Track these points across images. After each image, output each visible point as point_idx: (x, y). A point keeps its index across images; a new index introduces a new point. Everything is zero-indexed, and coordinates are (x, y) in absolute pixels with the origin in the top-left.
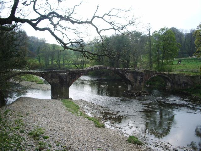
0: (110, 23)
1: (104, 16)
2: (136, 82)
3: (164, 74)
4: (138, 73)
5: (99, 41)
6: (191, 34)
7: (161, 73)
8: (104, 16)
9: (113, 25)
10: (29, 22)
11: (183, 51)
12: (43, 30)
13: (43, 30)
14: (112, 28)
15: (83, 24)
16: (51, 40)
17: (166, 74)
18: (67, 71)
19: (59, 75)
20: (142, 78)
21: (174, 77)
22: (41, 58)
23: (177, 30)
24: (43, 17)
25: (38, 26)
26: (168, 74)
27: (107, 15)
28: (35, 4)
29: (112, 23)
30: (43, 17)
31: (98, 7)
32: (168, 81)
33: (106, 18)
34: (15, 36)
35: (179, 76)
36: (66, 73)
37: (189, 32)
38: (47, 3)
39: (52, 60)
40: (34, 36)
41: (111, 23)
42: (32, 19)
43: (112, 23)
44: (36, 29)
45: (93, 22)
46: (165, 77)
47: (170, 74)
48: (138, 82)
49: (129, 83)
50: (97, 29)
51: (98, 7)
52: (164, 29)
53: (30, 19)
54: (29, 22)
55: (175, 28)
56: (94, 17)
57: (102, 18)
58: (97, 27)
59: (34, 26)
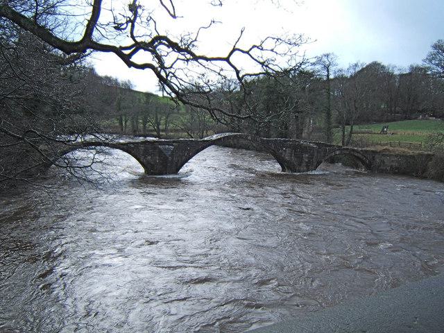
0: (260, 63)
1: (251, 49)
2: (300, 165)
3: (354, 150)
4: (305, 149)
5: (232, 88)
6: (410, 74)
7: (347, 149)
8: (251, 49)
9: (267, 66)
10: (118, 51)
11: (393, 109)
12: (143, 67)
13: (143, 67)
14: (264, 71)
15: (213, 62)
16: (146, 82)
17: (358, 152)
18: (174, 142)
19: (160, 149)
20: (312, 158)
21: (374, 157)
22: (124, 118)
23: (383, 67)
24: (138, 46)
25: (134, 59)
26: (362, 150)
27: (258, 47)
28: (133, 26)
29: (264, 62)
30: (138, 46)
31: (242, 32)
32: (360, 164)
33: (255, 52)
34: (76, 75)
35: (383, 155)
36: (172, 145)
37: (408, 72)
38: (149, 18)
39: (145, 123)
40: (109, 76)
41: (262, 64)
42: (123, 46)
43: (264, 62)
44: (130, 64)
45: (231, 59)
46: (355, 156)
47: (366, 151)
48: (304, 164)
49: (287, 167)
50: (238, 72)
51: (242, 32)
52: (356, 65)
53: (118, 46)
54: (118, 51)
55: (379, 64)
56: (234, 50)
57: (247, 53)
58: (239, 69)
59: (127, 60)
